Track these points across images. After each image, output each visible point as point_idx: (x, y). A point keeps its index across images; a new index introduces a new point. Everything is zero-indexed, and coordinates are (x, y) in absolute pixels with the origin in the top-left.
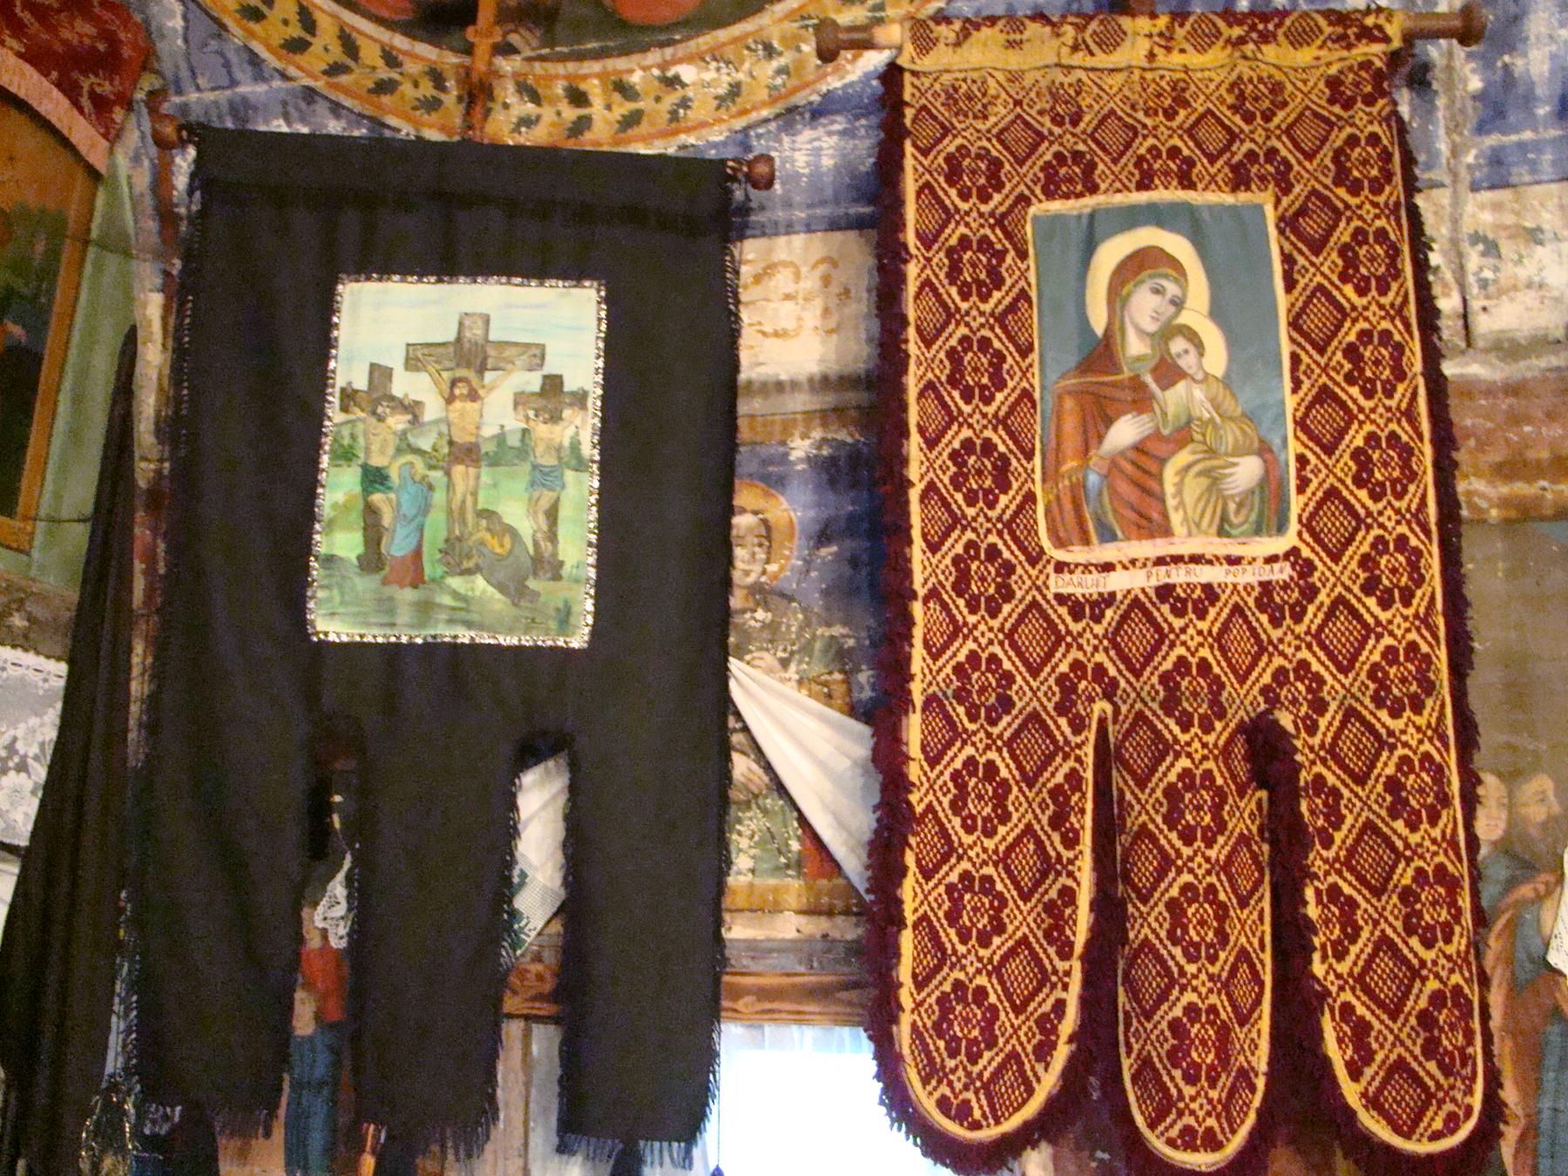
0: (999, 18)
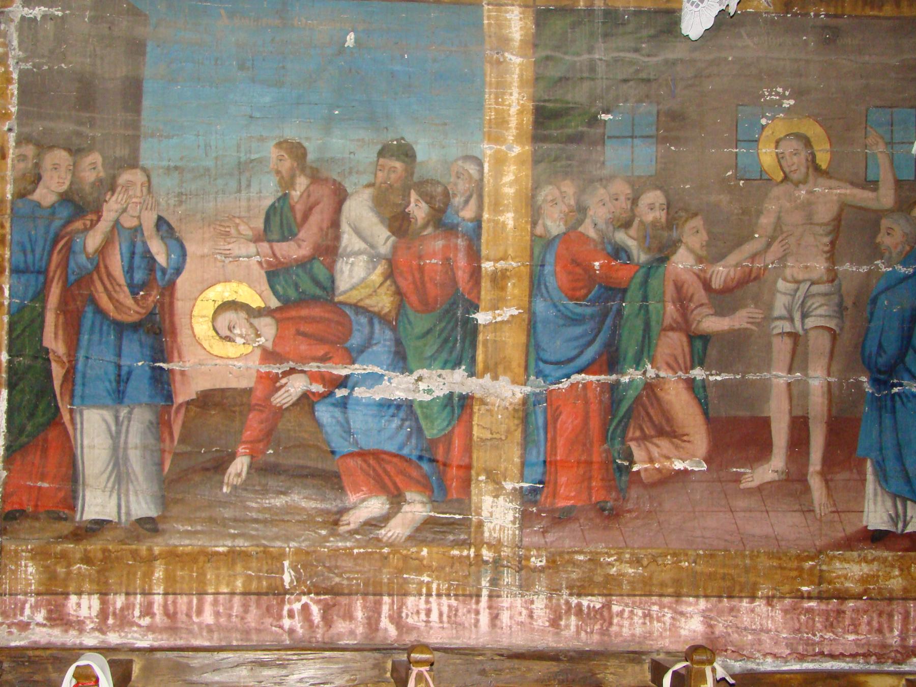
0: (750, 492)
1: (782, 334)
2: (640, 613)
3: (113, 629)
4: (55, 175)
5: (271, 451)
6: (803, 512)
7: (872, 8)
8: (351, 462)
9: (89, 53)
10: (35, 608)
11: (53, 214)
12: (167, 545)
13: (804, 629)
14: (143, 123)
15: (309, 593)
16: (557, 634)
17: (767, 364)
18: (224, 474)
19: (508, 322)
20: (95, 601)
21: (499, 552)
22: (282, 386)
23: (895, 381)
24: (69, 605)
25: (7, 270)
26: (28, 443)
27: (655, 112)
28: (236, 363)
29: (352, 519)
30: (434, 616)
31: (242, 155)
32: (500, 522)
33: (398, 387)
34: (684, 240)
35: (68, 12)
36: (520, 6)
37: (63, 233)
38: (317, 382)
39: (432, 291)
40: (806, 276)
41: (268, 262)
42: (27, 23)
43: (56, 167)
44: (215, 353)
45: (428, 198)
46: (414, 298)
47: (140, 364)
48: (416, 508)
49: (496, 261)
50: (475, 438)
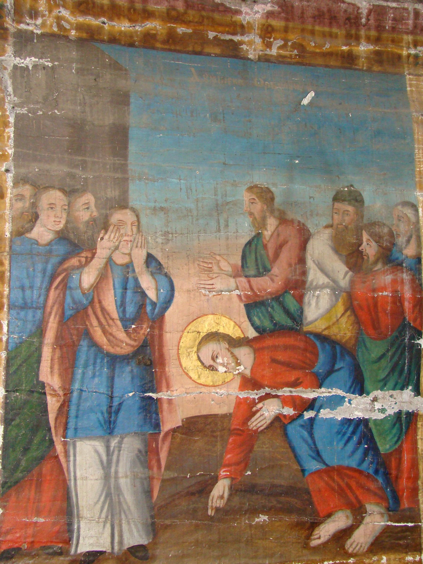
4: (52, 213)
9: (79, 101)
14: (130, 167)
18: (208, 497)
22: (257, 411)
25: (6, 306)
26: (23, 478)
33: (357, 407)
35: (56, 63)
41: (247, 296)
45: (377, 238)
47: (131, 394)
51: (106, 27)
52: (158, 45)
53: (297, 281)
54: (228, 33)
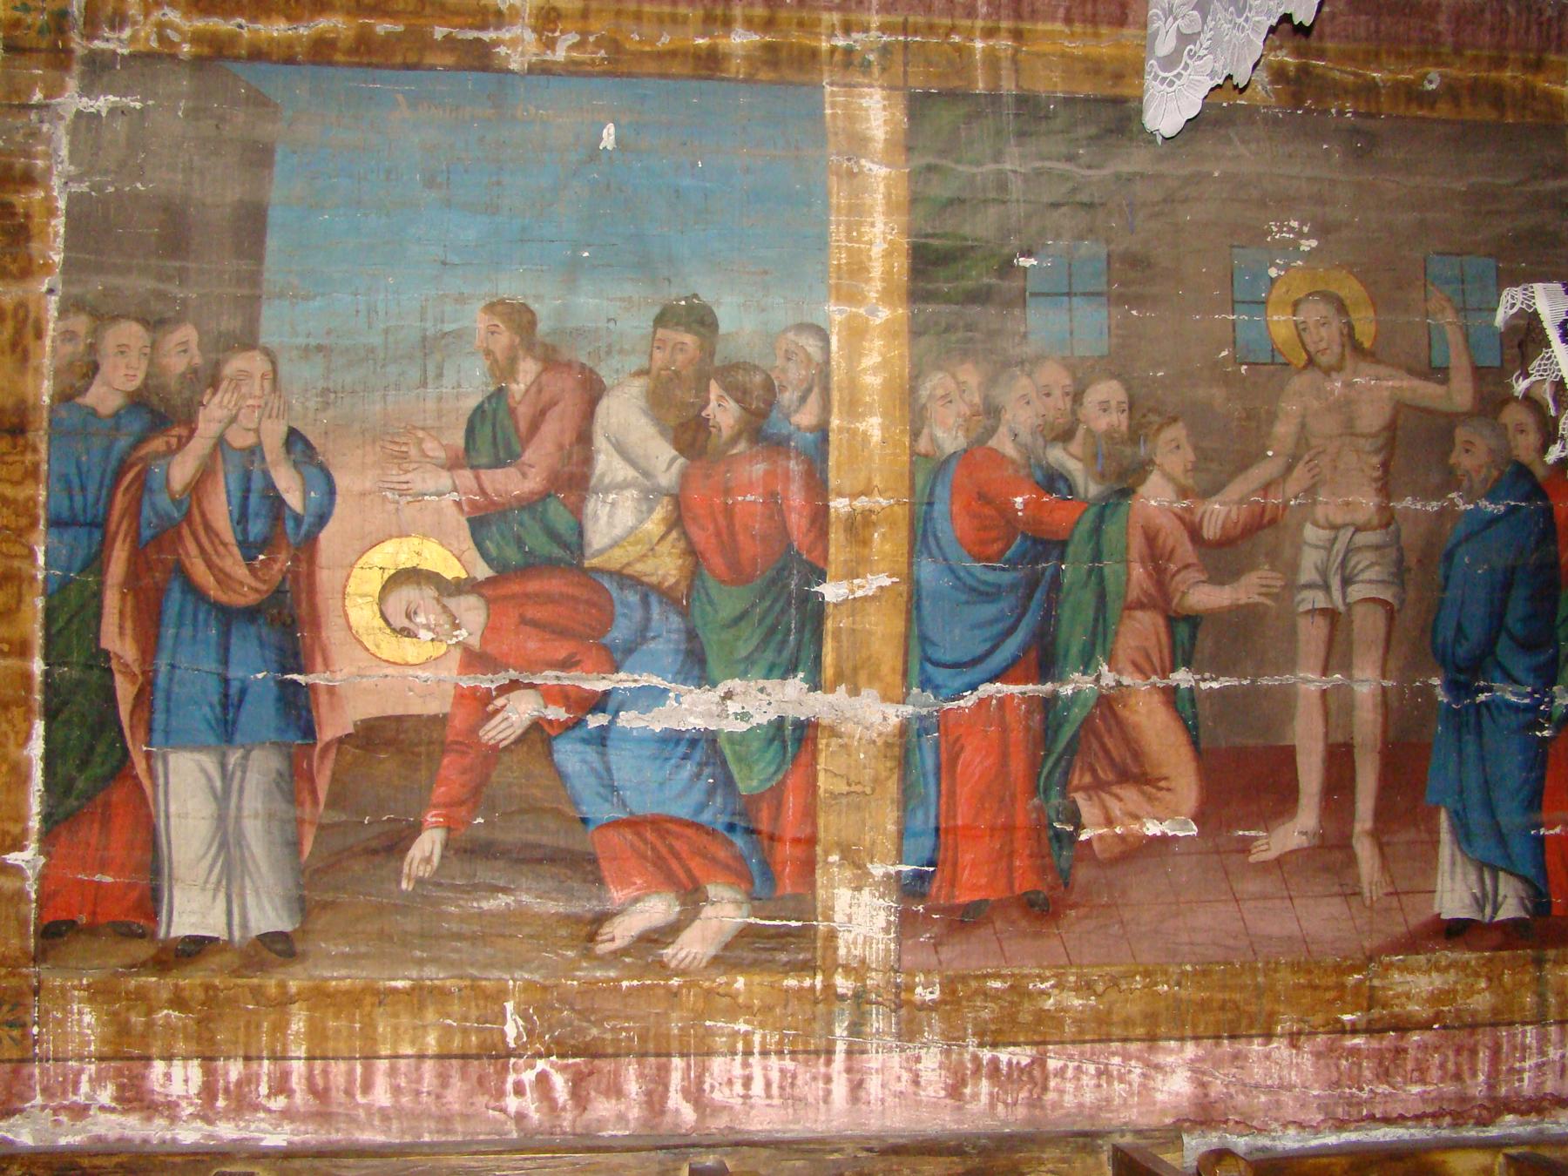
0: (1265, 867)
1: (1312, 612)
2: (1092, 1069)
3: (226, 1115)
4: (122, 361)
5: (480, 820)
6: (1346, 896)
7: (1421, 106)
8: (614, 836)
10: (97, 1081)
11: (117, 428)
12: (311, 978)
13: (1345, 1081)
14: (266, 275)
15: (549, 1055)
16: (960, 1108)
17: (1289, 663)
18: (402, 859)
19: (873, 598)
20: (195, 1070)
21: (863, 980)
22: (497, 711)
23: (1482, 683)
24: (153, 1076)
25: (42, 522)
26: (79, 808)
27: (1104, 256)
28: (419, 673)
29: (618, 932)
30: (757, 1087)
31: (429, 324)
32: (863, 930)
33: (692, 709)
34: (1158, 460)
35: (150, 102)
36: (882, 87)
37: (132, 459)
38: (555, 703)
39: (750, 549)
40: (1348, 519)
41: (472, 503)
42: (85, 120)
43: (122, 350)
44: (384, 657)
45: (739, 393)
46: (717, 561)
48: (725, 912)
49: (854, 496)
50: (821, 792)
51: (245, 33)
52: (339, 57)
53: (571, 476)
54: (471, 27)
